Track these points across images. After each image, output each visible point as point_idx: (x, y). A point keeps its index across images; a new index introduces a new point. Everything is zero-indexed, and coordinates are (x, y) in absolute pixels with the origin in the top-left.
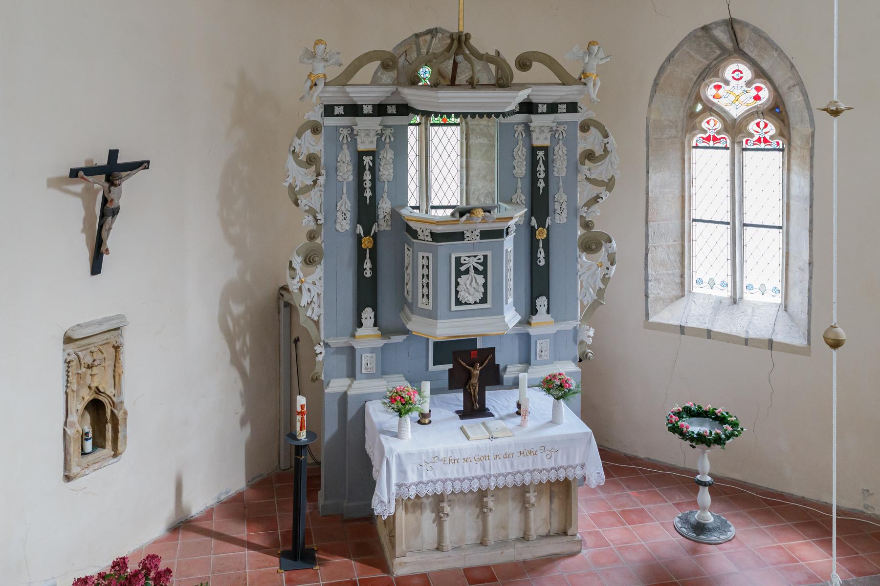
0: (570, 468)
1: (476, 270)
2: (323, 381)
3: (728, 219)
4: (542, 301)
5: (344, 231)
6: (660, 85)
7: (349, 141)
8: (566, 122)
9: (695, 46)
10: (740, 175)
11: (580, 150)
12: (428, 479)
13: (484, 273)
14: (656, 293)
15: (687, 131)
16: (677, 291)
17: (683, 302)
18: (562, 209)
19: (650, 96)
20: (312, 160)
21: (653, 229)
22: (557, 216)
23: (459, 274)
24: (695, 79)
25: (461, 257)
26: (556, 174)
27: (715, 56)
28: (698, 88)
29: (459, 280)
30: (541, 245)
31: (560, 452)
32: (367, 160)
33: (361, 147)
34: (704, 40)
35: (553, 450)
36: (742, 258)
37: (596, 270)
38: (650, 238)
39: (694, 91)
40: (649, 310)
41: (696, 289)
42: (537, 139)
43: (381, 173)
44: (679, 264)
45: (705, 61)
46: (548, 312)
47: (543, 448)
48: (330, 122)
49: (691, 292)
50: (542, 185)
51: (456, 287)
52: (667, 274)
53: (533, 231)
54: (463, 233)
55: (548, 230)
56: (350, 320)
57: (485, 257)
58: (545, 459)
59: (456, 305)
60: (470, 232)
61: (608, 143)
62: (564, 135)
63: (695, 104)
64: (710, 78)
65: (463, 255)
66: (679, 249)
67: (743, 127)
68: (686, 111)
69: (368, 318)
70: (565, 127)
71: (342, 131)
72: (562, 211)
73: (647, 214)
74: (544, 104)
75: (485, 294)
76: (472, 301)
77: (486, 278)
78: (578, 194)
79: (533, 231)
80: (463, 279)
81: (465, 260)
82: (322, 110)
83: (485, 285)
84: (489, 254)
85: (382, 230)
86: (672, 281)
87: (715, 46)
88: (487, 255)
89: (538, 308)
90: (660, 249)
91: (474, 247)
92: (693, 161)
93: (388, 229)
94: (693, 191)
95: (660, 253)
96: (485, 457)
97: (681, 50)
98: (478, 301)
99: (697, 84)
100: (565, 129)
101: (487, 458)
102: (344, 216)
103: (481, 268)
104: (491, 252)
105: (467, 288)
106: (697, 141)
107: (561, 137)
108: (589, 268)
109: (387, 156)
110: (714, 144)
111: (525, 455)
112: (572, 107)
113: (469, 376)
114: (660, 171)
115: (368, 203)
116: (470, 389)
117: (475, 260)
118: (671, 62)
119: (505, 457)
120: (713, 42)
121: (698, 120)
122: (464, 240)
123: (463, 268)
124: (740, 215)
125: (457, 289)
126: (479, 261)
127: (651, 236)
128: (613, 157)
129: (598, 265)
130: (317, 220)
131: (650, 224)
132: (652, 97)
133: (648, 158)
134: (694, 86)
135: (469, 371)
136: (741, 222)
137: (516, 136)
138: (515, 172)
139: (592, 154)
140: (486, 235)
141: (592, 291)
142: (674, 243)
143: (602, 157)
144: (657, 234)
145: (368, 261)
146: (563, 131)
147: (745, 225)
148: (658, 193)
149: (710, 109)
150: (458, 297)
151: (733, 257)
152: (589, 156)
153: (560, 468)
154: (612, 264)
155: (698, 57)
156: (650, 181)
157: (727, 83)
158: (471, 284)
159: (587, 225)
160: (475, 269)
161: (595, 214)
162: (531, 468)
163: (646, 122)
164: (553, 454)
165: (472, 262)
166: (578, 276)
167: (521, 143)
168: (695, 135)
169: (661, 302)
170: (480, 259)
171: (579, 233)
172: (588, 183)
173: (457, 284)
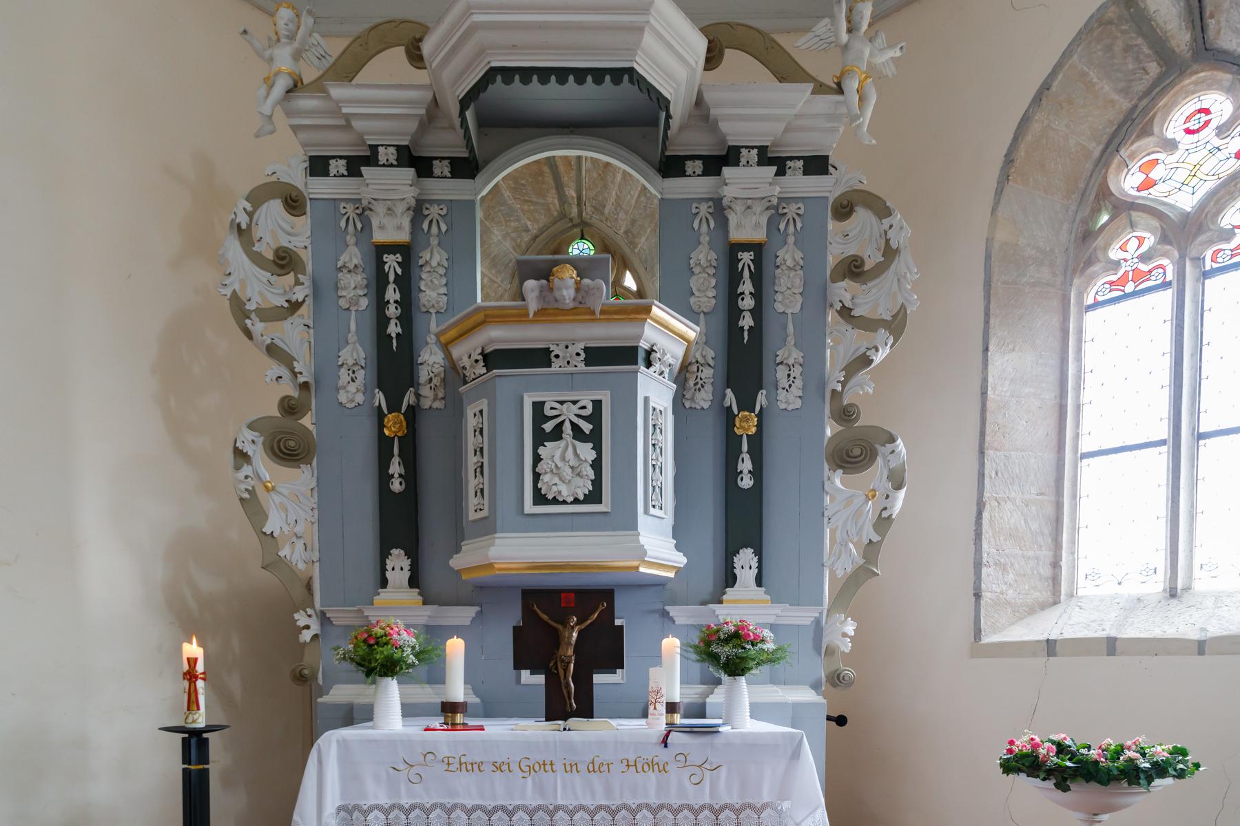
0: (748, 811)
1: (578, 433)
2: (321, 686)
3: (1163, 432)
4: (746, 560)
5: (352, 405)
6: (1017, 163)
7: (359, 229)
8: (803, 198)
9: (1099, 53)
10: (1195, 328)
11: (831, 261)
12: (411, 801)
13: (595, 439)
14: (998, 590)
15: (1074, 272)
16: (1044, 593)
17: (1057, 610)
18: (791, 378)
19: (996, 193)
20: (284, 262)
21: (994, 465)
22: (782, 395)
23: (540, 438)
24: (1097, 153)
25: (545, 402)
26: (779, 307)
27: (1147, 81)
28: (1104, 171)
29: (541, 450)
30: (745, 447)
31: (723, 771)
32: (392, 262)
33: (379, 237)
34: (1124, 32)
35: (706, 766)
36: (1192, 506)
37: (862, 505)
38: (987, 481)
39: (1095, 181)
40: (982, 622)
41: (1085, 588)
42: (739, 226)
43: (422, 295)
44: (1050, 541)
45: (1122, 100)
46: (759, 581)
47: (681, 758)
48: (321, 188)
49: (1072, 596)
50: (747, 322)
51: (535, 465)
52: (1023, 556)
53: (729, 417)
54: (547, 351)
55: (760, 416)
56: (372, 576)
57: (597, 404)
58: (687, 783)
59: (535, 503)
60: (562, 346)
61: (891, 227)
62: (799, 225)
63: (1096, 211)
64: (1132, 143)
65: (549, 398)
66: (1050, 510)
67: (1209, 216)
68: (1074, 230)
69: (397, 569)
70: (799, 208)
71: (344, 208)
72: (791, 382)
73: (983, 434)
74: (753, 147)
75: (597, 482)
76: (566, 493)
77: (598, 448)
78: (828, 351)
79: (729, 417)
80: (549, 450)
81: (552, 408)
82: (307, 164)
83: (597, 465)
84: (605, 397)
85: (427, 406)
86: (1033, 573)
87: (1146, 50)
88: (601, 401)
89: (737, 571)
90: (1009, 506)
91: (571, 381)
92: (1087, 336)
93: (437, 405)
94: (1085, 397)
95: (1009, 514)
96: (544, 765)
97: (1066, 67)
98: (581, 497)
99: (1100, 165)
100: (801, 212)
101: (548, 767)
102: (351, 374)
103: (587, 427)
104: (609, 393)
105: (556, 465)
106: (1097, 293)
107: (791, 229)
108: (849, 500)
109: (433, 258)
110: (1136, 287)
111: (640, 769)
112: (817, 165)
113: (556, 640)
114: (1013, 350)
115: (394, 348)
116: (556, 668)
117: (575, 409)
118: (1044, 102)
119: (591, 769)
120: (1145, 36)
121: (1100, 241)
122: (550, 367)
123: (548, 427)
124: (1192, 414)
125: (537, 470)
126: (583, 412)
127: (991, 477)
128: (905, 264)
129: (867, 496)
130: (295, 374)
131: (990, 453)
132: (999, 192)
133: (987, 322)
134: (1094, 171)
135: (556, 630)
136: (1194, 429)
137: (696, 225)
138: (692, 300)
139: (857, 261)
140: (596, 356)
141: (854, 550)
142: (1040, 497)
143: (881, 269)
144: (1002, 473)
145: (396, 460)
146: (796, 217)
147: (1201, 436)
148: (1008, 394)
149: (1125, 209)
150: (539, 486)
151: (1173, 502)
152: (853, 269)
153: (724, 807)
154: (898, 487)
155: (1106, 88)
156: (990, 368)
157: (1171, 145)
158: (563, 458)
159: (845, 415)
160: (575, 427)
161: (862, 389)
162: (653, 800)
163: (986, 248)
164: (707, 773)
165: (569, 413)
166: (826, 520)
167: (705, 239)
168: (1092, 278)
169: (1009, 610)
170: (584, 407)
171: (829, 432)
172: (849, 328)
173: (537, 459)
